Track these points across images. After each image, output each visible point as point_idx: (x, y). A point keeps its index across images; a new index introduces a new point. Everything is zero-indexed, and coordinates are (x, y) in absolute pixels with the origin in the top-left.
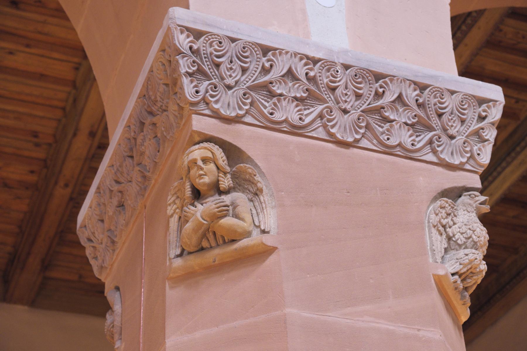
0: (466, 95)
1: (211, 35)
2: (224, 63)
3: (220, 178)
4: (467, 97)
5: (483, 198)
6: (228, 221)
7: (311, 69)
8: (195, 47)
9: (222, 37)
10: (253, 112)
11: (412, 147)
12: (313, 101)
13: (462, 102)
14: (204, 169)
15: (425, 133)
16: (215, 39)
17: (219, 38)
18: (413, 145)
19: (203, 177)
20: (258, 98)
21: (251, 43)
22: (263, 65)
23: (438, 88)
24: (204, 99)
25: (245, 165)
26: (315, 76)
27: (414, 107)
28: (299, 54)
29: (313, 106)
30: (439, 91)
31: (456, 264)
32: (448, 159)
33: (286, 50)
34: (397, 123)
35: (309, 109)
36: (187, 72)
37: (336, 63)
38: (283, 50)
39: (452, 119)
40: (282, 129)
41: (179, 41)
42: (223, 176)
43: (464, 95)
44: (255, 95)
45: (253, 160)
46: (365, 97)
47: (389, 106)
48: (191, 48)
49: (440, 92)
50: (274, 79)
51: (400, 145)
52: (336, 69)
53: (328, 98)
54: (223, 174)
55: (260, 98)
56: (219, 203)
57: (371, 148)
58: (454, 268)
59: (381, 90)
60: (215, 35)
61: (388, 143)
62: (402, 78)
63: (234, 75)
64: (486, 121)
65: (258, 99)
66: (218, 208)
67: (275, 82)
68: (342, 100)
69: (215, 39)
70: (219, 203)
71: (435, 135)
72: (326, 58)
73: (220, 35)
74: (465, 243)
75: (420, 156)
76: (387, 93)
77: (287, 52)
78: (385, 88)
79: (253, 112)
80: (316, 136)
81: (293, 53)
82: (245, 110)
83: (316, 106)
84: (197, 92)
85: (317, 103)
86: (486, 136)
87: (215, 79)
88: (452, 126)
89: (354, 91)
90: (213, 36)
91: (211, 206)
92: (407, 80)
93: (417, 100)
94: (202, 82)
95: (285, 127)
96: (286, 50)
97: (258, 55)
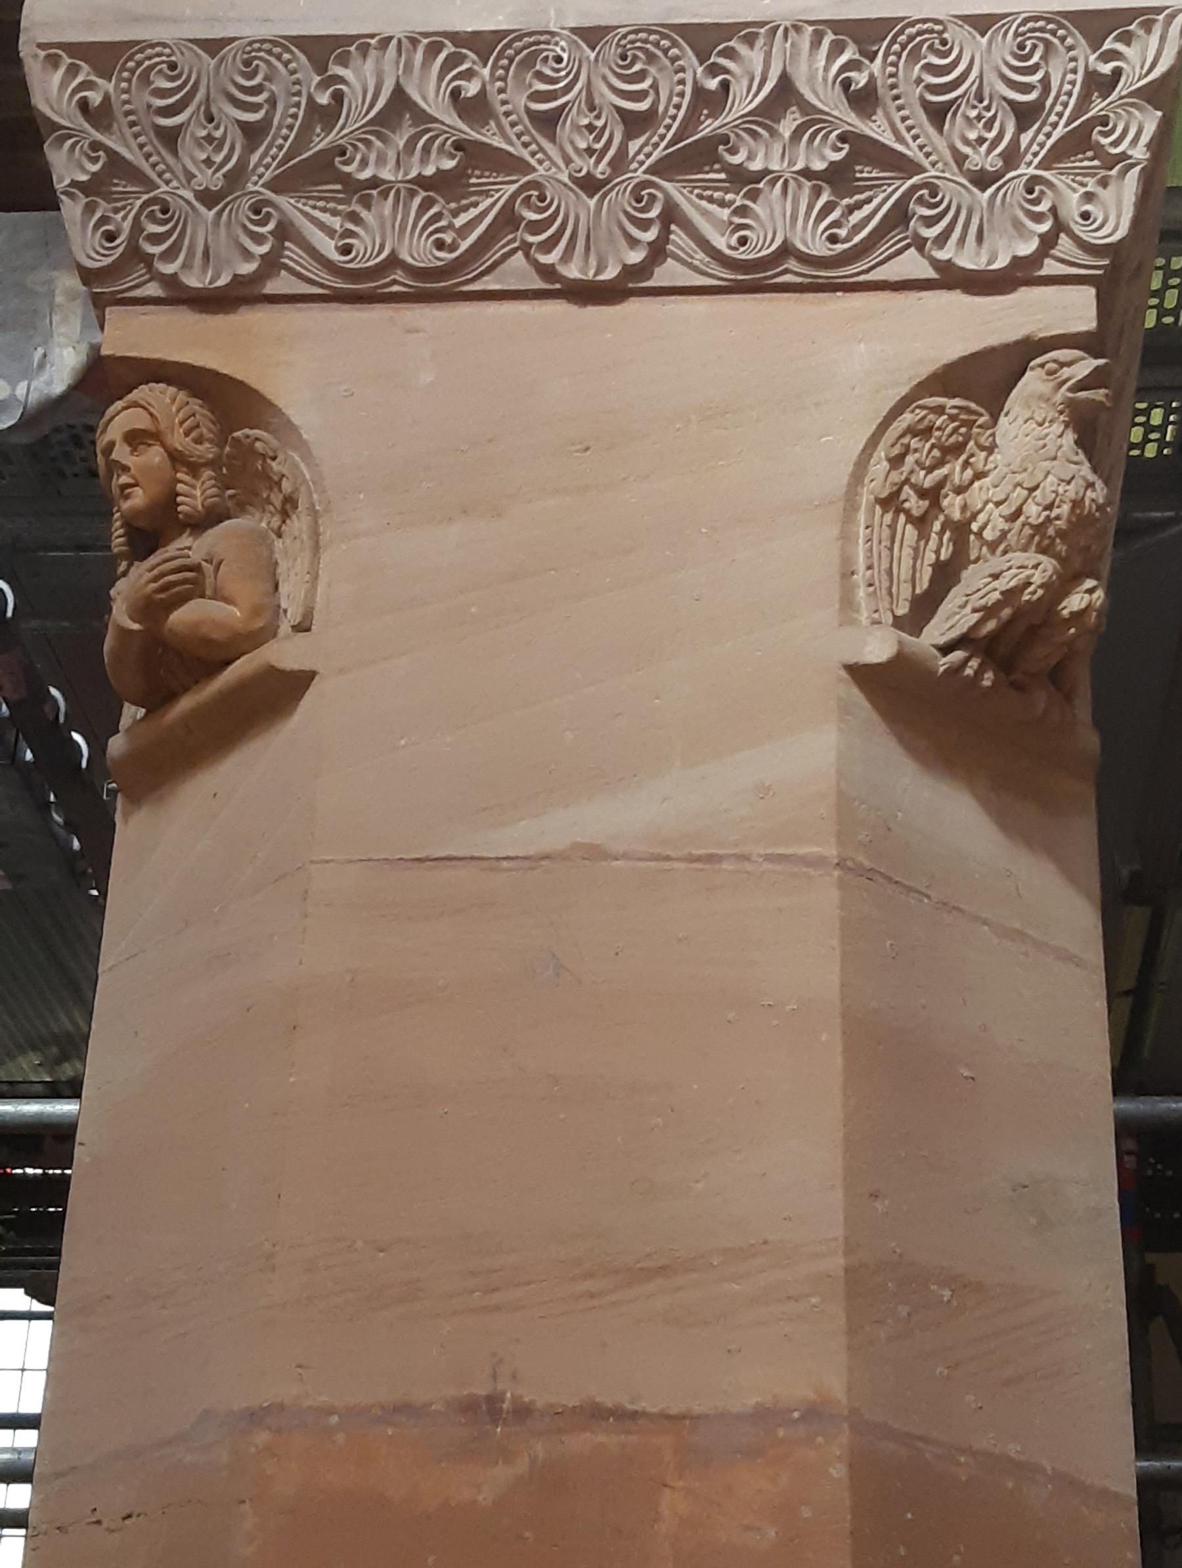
0: (1036, 19)
1: (141, 51)
2: (186, 129)
3: (180, 487)
4: (1041, 23)
5: (1086, 366)
6: (182, 616)
7: (469, 75)
8: (95, 98)
9: (174, 48)
10: (291, 259)
11: (830, 249)
12: (488, 177)
13: (1021, 47)
14: (132, 469)
15: (885, 187)
16: (157, 60)
17: (167, 51)
18: (833, 239)
19: (129, 494)
20: (307, 209)
21: (270, 41)
22: (311, 100)
23: (925, 21)
24: (134, 255)
25: (247, 431)
26: (483, 92)
27: (836, 113)
28: (426, 35)
29: (487, 194)
30: (932, 31)
31: (959, 613)
32: (969, 260)
33: (378, 34)
34: (773, 182)
35: (475, 205)
36: (74, 184)
37: (553, 34)
38: (372, 36)
39: (979, 118)
40: (387, 290)
41: (48, 101)
42: (187, 478)
43: (1025, 21)
44: (295, 204)
45: (280, 410)
46: (664, 119)
47: (745, 130)
48: (84, 105)
49: (935, 35)
50: (345, 139)
51: (786, 250)
52: (551, 54)
53: (533, 154)
54: (187, 474)
55: (314, 207)
56: (159, 565)
57: (698, 283)
58: (952, 627)
59: (713, 84)
60: (152, 46)
61: (741, 254)
62: (788, 24)
63: (218, 159)
64: (1121, 89)
65: (306, 214)
66: (155, 579)
67: (350, 147)
68: (576, 150)
69: (157, 60)
70: (159, 565)
71: (914, 188)
72: (515, 27)
73: (168, 42)
74: (1004, 534)
75: (867, 271)
76: (738, 88)
77: (385, 42)
78: (727, 71)
79: (291, 259)
80: (497, 287)
81: (406, 37)
82: (259, 258)
83: (497, 191)
84: (111, 237)
85: (499, 179)
86: (1116, 143)
87: (167, 183)
88: (981, 140)
89: (619, 110)
90: (149, 51)
91: (141, 576)
92: (806, 25)
93: (846, 84)
94: (130, 201)
95: (399, 282)
96: (378, 34)
97: (669, 49)
